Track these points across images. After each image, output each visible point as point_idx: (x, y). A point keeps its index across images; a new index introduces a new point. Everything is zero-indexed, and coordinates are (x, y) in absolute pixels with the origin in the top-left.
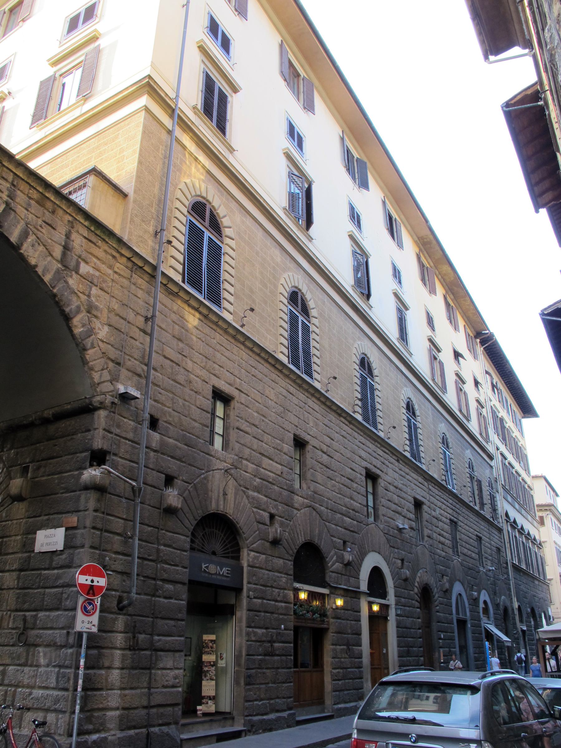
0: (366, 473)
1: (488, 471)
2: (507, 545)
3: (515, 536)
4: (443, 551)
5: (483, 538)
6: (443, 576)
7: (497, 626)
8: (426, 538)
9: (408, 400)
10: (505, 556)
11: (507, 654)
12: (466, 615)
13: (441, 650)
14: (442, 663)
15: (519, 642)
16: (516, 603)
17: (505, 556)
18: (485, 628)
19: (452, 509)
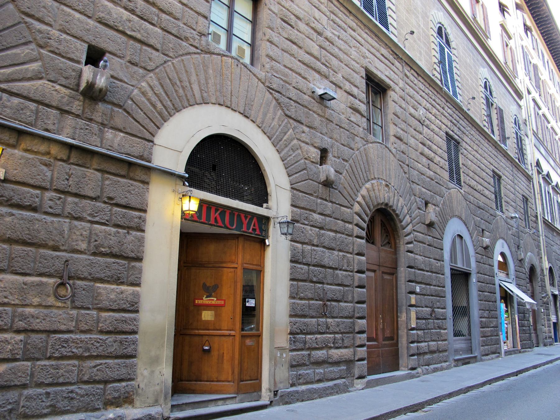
0: (366, 75)
1: (514, 107)
2: (538, 196)
3: (548, 192)
4: (429, 168)
5: (503, 177)
6: (426, 204)
7: (519, 286)
8: (392, 139)
9: (485, 80)
10: (534, 208)
11: (531, 320)
12: (469, 264)
13: (413, 310)
14: (413, 329)
15: (548, 307)
16: (547, 262)
17: (534, 208)
18: (500, 286)
19: (451, 121)
